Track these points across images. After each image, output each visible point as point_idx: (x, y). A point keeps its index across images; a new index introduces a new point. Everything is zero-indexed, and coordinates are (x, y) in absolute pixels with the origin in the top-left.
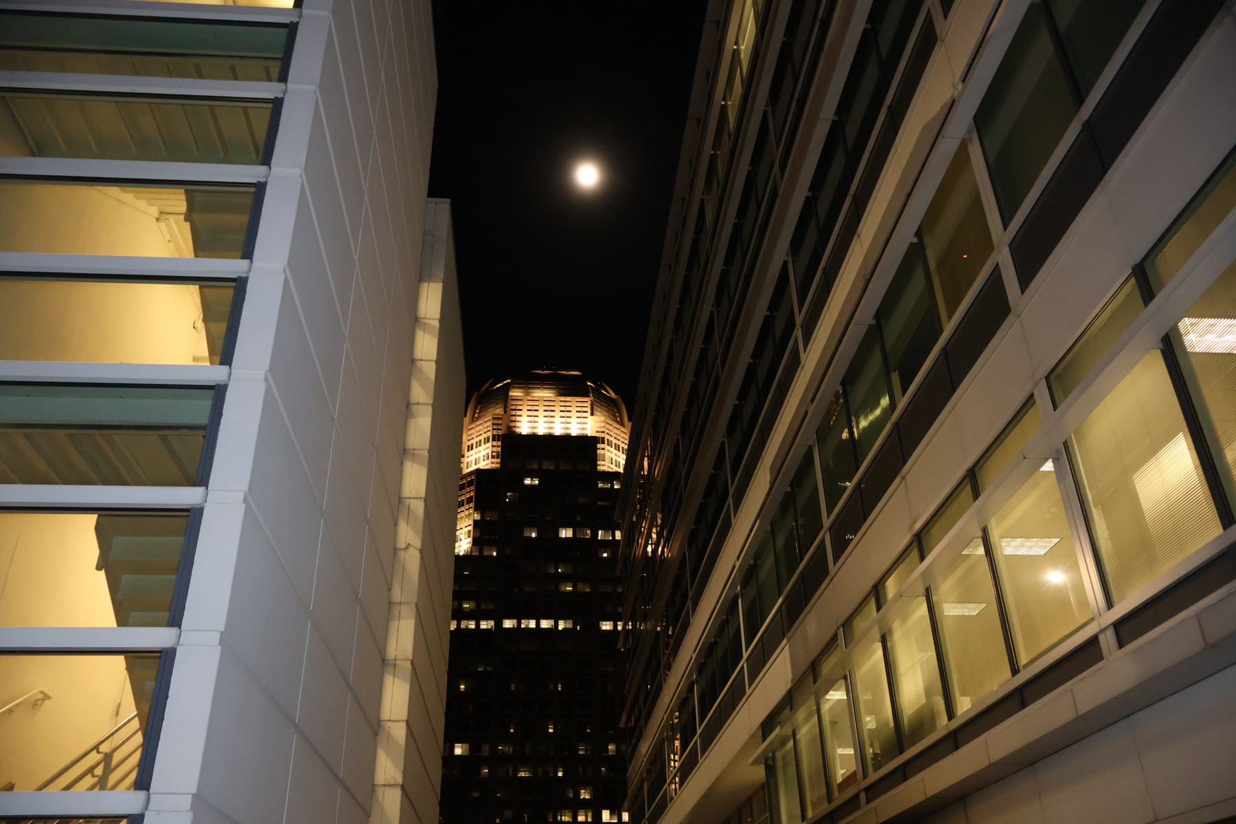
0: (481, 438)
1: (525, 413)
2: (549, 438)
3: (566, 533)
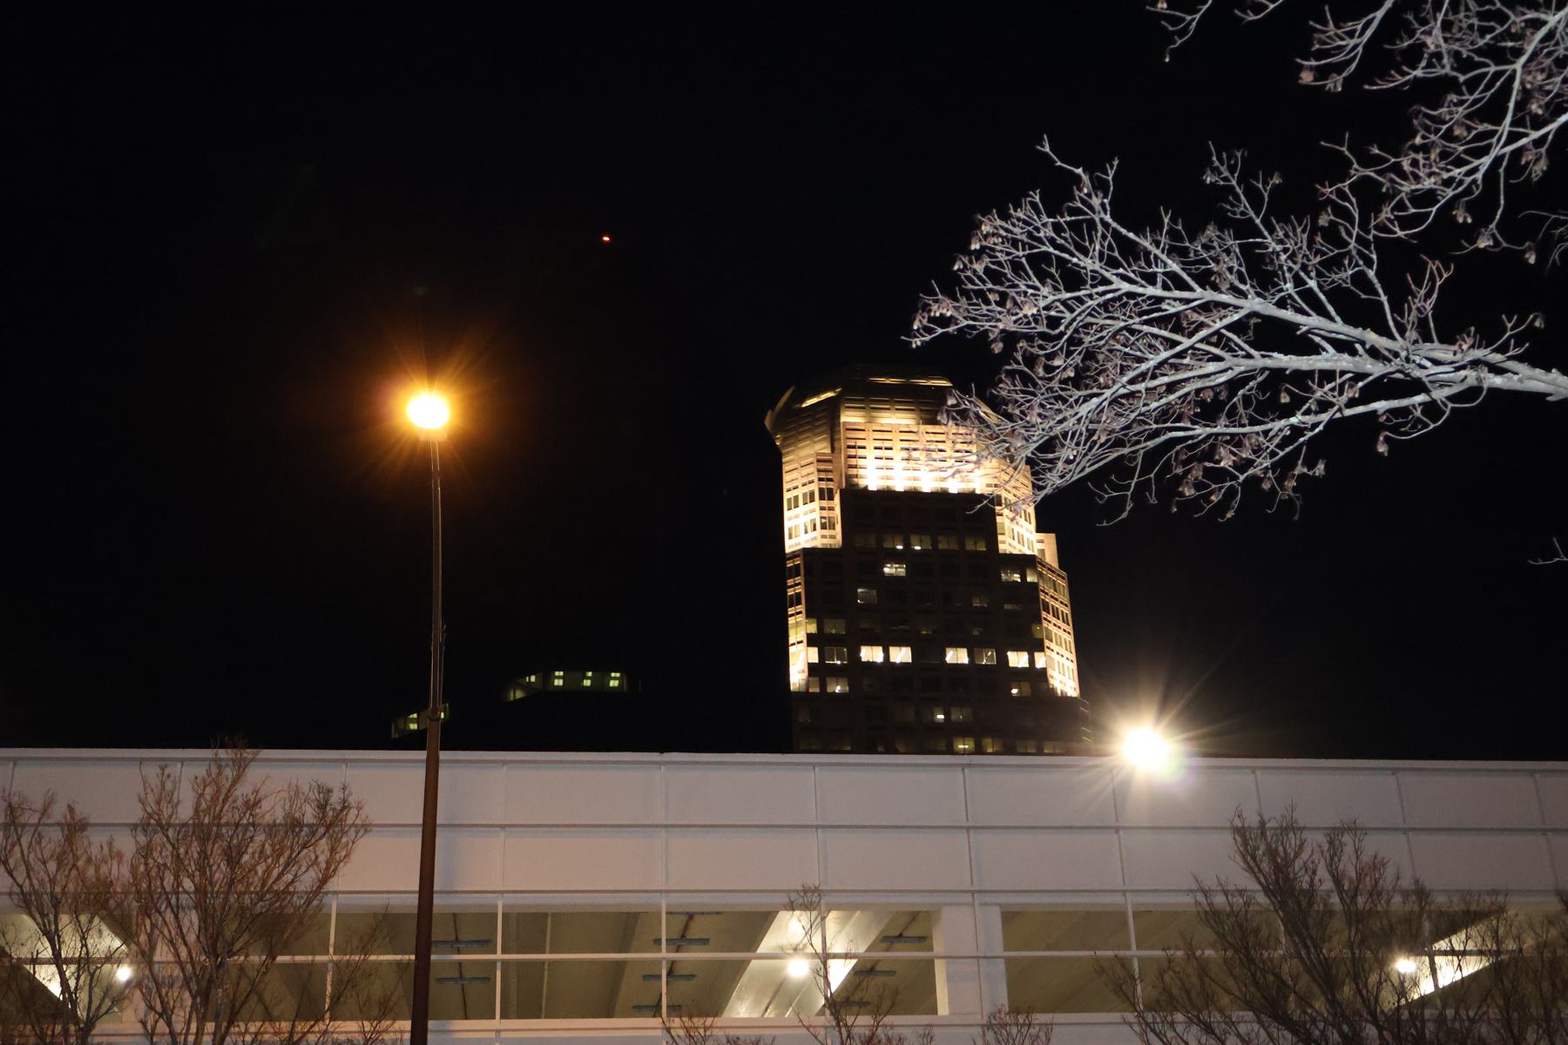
0: (800, 492)
1: (870, 453)
2: (913, 496)
3: (957, 656)
